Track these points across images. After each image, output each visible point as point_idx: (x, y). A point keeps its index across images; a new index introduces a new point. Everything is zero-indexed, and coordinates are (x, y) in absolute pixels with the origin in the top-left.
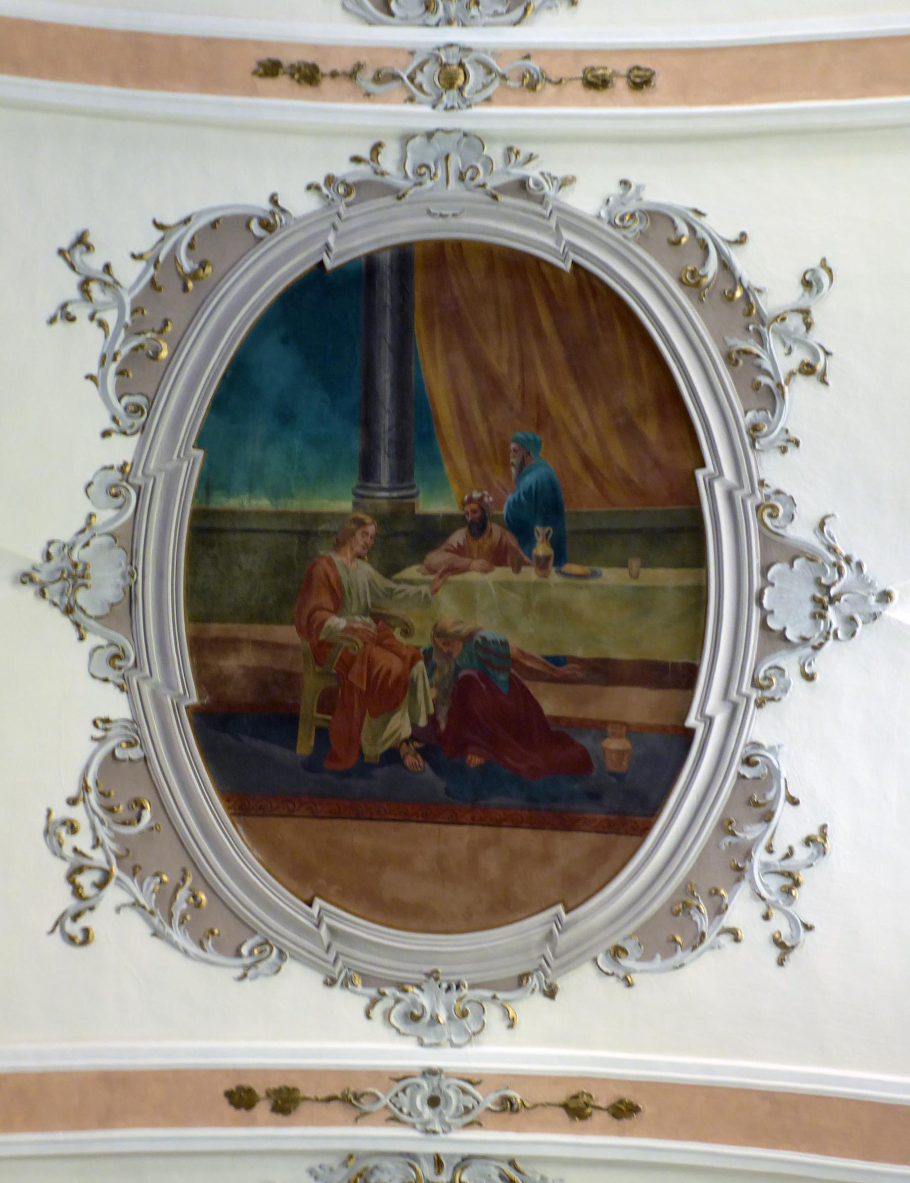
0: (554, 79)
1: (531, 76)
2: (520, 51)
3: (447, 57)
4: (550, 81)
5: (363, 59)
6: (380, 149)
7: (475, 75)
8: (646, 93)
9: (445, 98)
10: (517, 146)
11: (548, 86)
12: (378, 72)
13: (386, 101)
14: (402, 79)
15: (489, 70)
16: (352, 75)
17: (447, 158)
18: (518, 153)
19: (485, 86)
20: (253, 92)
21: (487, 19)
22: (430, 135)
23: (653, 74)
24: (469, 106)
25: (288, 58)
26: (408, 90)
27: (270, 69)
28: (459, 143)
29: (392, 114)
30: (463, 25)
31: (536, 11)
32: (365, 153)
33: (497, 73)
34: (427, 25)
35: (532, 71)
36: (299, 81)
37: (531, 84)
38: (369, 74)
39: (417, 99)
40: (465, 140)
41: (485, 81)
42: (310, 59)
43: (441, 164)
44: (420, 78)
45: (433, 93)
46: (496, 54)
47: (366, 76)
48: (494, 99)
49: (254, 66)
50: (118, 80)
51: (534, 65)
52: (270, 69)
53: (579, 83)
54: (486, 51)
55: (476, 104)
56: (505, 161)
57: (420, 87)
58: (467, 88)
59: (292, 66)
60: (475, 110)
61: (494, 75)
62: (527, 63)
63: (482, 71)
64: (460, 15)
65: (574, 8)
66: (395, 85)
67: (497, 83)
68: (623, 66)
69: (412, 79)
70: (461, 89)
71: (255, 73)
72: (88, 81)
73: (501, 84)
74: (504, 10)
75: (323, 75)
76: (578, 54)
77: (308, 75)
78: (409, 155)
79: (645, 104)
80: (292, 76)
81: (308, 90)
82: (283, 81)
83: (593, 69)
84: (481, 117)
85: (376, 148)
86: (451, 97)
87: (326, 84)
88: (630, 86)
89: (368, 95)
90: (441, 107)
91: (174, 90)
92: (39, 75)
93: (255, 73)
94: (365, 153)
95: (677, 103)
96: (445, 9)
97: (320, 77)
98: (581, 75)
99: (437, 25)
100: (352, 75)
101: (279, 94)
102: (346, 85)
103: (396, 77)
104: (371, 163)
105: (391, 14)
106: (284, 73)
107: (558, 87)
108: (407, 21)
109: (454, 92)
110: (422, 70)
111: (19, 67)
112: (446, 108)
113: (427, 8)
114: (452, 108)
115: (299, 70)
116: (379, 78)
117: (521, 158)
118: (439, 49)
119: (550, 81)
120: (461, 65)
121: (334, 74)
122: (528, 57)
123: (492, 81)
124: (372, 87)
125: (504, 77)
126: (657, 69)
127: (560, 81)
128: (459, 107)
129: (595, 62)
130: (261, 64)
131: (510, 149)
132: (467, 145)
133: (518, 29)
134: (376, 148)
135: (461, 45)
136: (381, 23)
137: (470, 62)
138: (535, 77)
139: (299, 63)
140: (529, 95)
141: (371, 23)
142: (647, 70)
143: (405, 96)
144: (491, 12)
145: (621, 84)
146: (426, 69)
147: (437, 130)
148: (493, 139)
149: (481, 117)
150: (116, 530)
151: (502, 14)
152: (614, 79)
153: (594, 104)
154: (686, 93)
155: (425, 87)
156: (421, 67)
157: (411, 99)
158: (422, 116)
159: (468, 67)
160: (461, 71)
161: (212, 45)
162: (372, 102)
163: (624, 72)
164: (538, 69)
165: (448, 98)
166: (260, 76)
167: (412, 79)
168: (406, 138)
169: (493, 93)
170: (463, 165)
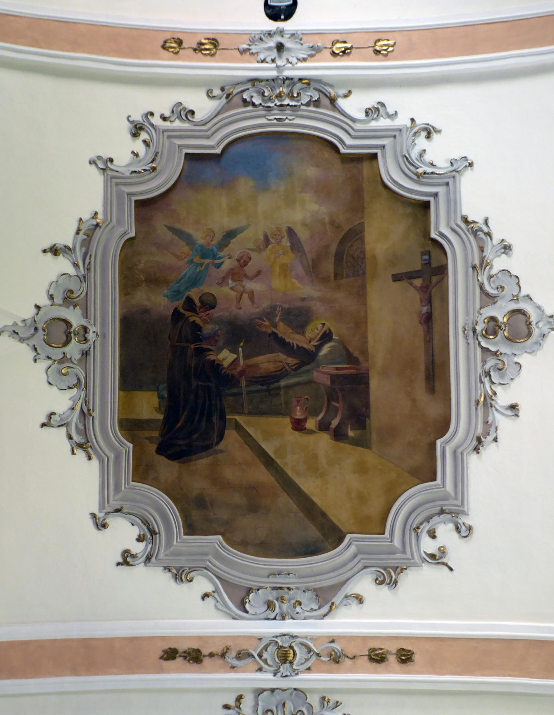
0: (350, 656)
1: (336, 653)
2: (329, 637)
3: (282, 641)
4: (348, 657)
5: (229, 643)
6: (242, 701)
7: (300, 653)
8: (409, 666)
9: (281, 669)
10: (328, 697)
11: (347, 660)
12: (239, 653)
13: (244, 672)
14: (254, 657)
15: (310, 650)
16: (223, 655)
17: (284, 704)
18: (328, 702)
19: (307, 660)
20: (161, 671)
21: (307, 614)
22: (273, 690)
23: (413, 653)
24: (297, 674)
25: (182, 647)
26: (259, 663)
27: (170, 654)
28: (291, 694)
29: (249, 678)
30: (293, 618)
31: (337, 607)
32: (232, 703)
33: (314, 652)
34: (268, 619)
35: (336, 651)
36: (189, 661)
37: (336, 659)
38: (233, 654)
39: (264, 670)
40: (295, 692)
41: (306, 657)
42: (195, 645)
43: (280, 707)
44: (265, 656)
45: (274, 666)
46: (313, 639)
47: (231, 659)
48: (312, 668)
49: (161, 653)
50: (75, 672)
51: (337, 646)
52: (170, 654)
53: (366, 657)
54: (306, 638)
55: (302, 672)
56: (321, 706)
57: (265, 661)
58: (295, 662)
59: (185, 652)
60: (302, 676)
61: (312, 653)
62: (332, 645)
63: (305, 650)
64: (289, 611)
65: (361, 605)
66: (249, 660)
67: (314, 658)
68: (393, 647)
69: (260, 656)
70: (291, 663)
71: (161, 658)
72: (57, 675)
73: (316, 659)
74: (317, 608)
75: (204, 656)
76: (365, 638)
77: (195, 657)
78: (260, 703)
79: (408, 673)
80: (185, 658)
81: (196, 666)
82: (179, 661)
83: (374, 650)
84: (306, 680)
85: (239, 699)
86: (285, 669)
87: (207, 661)
88: (398, 661)
89: (233, 667)
90: (279, 675)
91: (110, 674)
92: (25, 676)
93: (161, 658)
94: (232, 703)
95: (429, 673)
96: (280, 607)
97: (202, 658)
98: (367, 653)
99: (275, 619)
100: (223, 655)
101: (177, 671)
102: (220, 662)
103: (250, 655)
104: (236, 709)
105: (247, 612)
106: (180, 656)
107: (353, 660)
108: (256, 617)
109: (288, 665)
110: (266, 650)
111: (12, 673)
112: (282, 676)
113: (269, 607)
114: (286, 676)
115: (189, 654)
116: (240, 656)
117: (331, 704)
118: (277, 637)
119: (348, 657)
120: (291, 647)
121: (211, 655)
122: (333, 641)
123: (311, 656)
124: (235, 662)
125: (318, 655)
126: (414, 650)
127: (354, 657)
128: (291, 676)
129: (376, 645)
130: (165, 652)
131: (323, 698)
132: (295, 695)
133: (326, 621)
134: (239, 699)
135: (291, 634)
136: (242, 618)
137: (296, 645)
138: (338, 654)
139: (189, 649)
140: (335, 666)
141: (234, 618)
142: (410, 651)
143: (257, 667)
144: (309, 609)
145: (392, 659)
146: (268, 650)
147: (277, 689)
148: (312, 691)
149: (306, 680)
150: (69, 363)
151: (315, 610)
152: (388, 656)
153: (376, 672)
154: (434, 667)
155: (269, 662)
156: (266, 648)
157: (260, 670)
158: (266, 679)
159: (296, 648)
160: (291, 651)
161: (134, 642)
162: (236, 672)
163: (394, 651)
164: (340, 649)
165: (284, 668)
166: (166, 659)
167: (260, 656)
168: (259, 692)
169: (312, 664)
170: (294, 709)
